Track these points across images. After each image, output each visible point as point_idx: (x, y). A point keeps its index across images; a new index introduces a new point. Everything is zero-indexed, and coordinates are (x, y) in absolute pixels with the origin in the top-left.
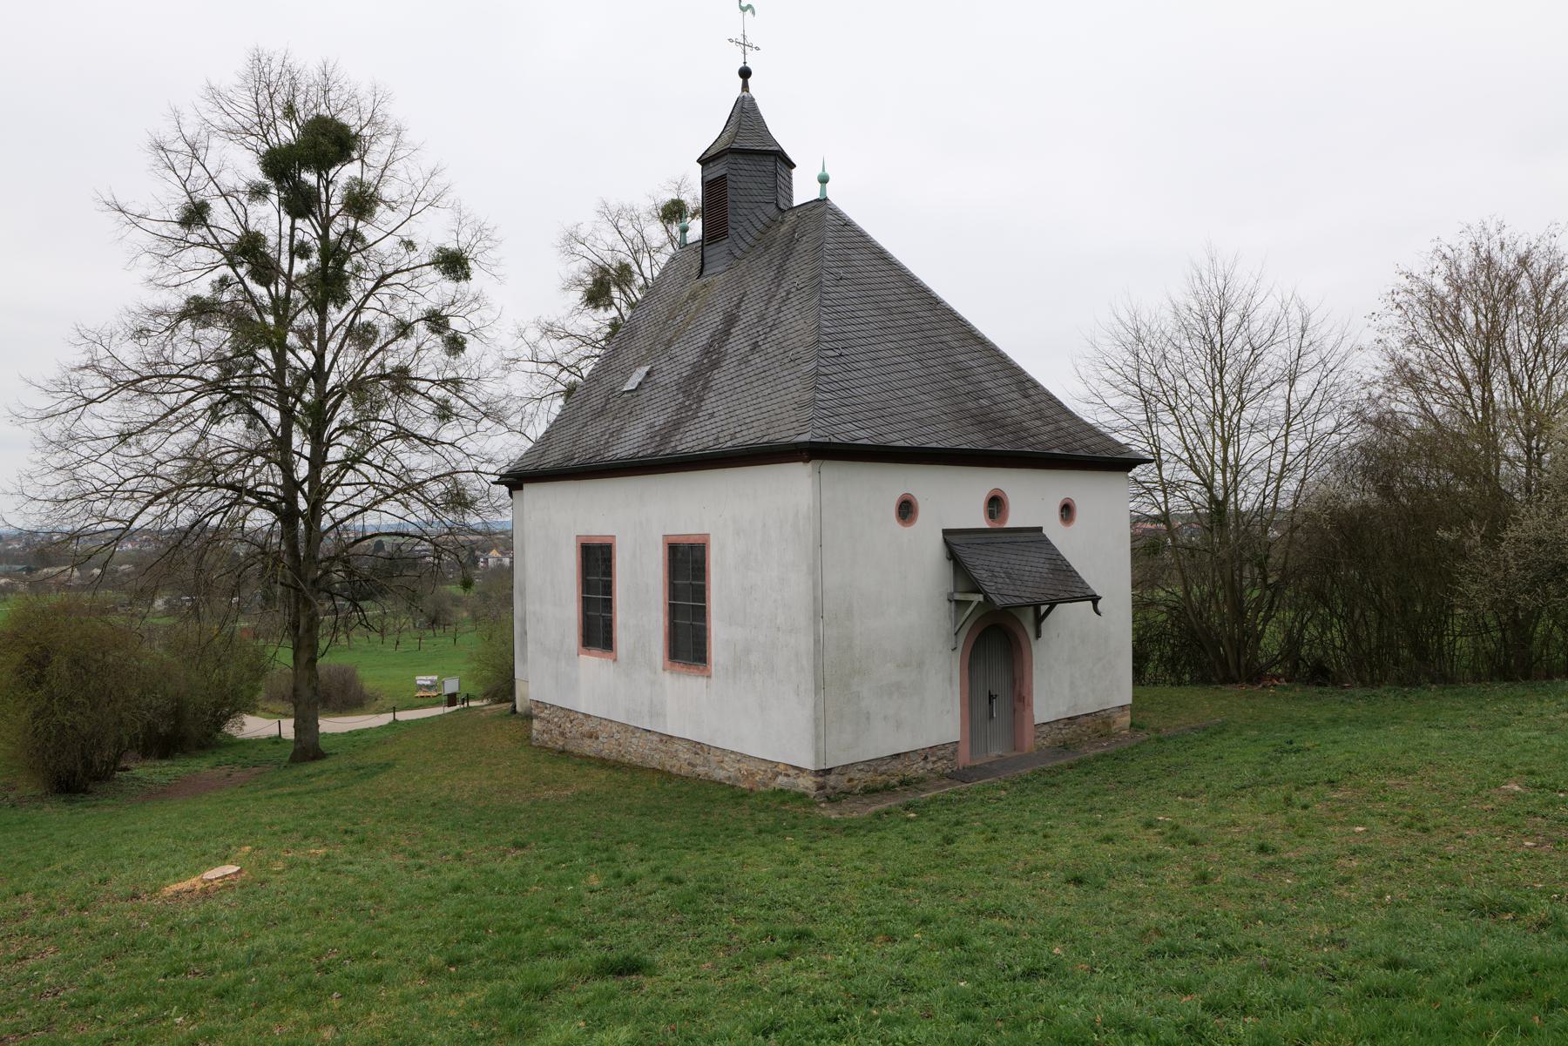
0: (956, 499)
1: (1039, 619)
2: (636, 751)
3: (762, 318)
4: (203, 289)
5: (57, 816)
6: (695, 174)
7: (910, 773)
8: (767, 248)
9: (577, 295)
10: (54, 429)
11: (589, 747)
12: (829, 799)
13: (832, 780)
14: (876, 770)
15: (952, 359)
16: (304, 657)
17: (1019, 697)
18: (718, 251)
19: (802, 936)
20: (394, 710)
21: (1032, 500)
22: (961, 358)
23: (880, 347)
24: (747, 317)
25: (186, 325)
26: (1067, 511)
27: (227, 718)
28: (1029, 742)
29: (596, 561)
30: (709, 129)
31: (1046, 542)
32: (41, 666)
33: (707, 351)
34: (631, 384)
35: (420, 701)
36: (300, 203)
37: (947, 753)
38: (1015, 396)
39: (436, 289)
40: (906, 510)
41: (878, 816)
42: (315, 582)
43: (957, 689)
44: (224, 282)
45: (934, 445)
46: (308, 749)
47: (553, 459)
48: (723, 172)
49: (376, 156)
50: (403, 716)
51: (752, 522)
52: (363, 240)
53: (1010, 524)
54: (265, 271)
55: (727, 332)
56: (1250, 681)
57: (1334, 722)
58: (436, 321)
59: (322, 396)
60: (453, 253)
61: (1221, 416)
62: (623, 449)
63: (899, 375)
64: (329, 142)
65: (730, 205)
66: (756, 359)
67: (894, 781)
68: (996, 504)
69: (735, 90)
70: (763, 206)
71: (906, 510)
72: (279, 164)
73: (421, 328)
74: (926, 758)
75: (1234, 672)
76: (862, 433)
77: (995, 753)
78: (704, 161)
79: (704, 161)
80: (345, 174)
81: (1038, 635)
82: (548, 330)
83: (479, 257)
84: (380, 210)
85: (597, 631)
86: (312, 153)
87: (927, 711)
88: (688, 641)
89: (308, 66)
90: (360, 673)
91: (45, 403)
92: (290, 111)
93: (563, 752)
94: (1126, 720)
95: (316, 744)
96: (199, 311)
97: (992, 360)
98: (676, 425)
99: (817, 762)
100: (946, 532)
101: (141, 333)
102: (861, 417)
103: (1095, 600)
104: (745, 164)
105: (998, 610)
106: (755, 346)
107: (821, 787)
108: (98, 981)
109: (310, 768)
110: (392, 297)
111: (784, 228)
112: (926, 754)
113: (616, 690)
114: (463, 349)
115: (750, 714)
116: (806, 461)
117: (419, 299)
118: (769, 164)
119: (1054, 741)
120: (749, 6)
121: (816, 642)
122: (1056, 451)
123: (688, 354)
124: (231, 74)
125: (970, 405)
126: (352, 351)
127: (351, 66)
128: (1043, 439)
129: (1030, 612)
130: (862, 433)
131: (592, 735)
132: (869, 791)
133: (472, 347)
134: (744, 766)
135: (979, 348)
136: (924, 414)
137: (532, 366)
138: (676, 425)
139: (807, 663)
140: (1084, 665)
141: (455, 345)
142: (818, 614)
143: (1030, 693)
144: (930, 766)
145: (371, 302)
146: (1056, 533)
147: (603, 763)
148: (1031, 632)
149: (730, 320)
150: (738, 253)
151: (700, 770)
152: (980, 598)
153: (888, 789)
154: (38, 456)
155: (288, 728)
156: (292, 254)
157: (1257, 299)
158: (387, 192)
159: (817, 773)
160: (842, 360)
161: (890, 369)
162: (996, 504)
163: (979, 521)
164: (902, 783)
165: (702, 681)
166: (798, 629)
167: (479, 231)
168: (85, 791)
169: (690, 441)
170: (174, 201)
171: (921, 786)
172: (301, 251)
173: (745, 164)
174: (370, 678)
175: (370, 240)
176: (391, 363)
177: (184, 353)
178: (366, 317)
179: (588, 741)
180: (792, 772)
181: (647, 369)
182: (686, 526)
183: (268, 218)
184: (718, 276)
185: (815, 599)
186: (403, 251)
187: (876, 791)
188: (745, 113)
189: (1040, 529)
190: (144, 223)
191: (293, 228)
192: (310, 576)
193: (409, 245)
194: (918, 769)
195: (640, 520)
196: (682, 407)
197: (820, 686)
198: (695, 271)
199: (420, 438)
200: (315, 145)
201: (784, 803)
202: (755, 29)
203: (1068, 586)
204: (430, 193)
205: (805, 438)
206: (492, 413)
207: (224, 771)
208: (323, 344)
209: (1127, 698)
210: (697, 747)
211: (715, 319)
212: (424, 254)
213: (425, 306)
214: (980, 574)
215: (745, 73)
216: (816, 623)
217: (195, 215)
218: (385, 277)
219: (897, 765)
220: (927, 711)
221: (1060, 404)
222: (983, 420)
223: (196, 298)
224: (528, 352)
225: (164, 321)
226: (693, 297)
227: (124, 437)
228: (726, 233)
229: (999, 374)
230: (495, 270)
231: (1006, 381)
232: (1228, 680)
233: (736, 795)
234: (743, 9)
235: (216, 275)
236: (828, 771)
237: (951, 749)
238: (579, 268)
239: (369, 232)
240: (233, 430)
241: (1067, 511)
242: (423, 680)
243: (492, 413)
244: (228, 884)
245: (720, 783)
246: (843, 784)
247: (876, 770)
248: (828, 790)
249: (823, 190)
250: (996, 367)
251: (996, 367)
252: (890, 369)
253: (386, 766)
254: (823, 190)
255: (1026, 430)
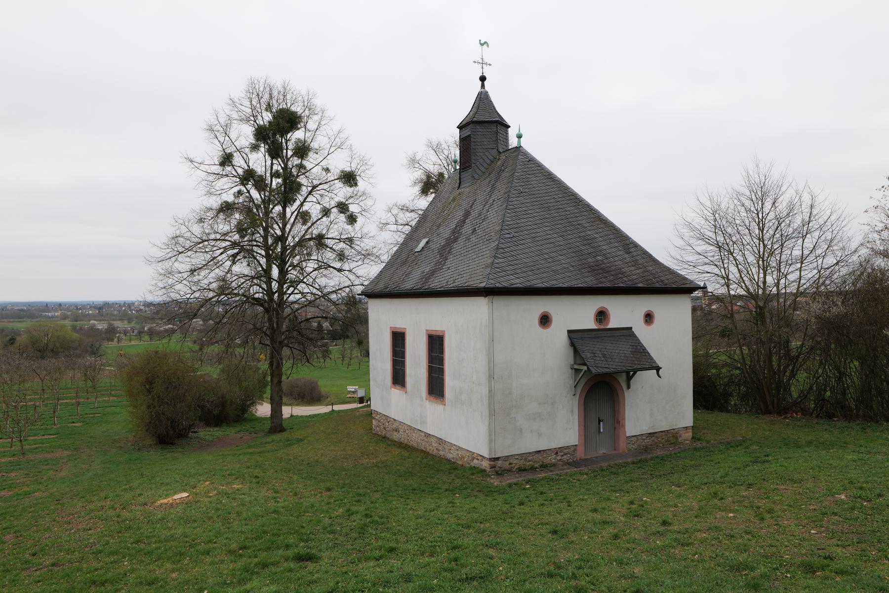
0: (579, 314)
1: (629, 378)
2: (415, 440)
3: (480, 215)
4: (230, 198)
5: (154, 455)
6: (455, 134)
7: (547, 461)
8: (490, 174)
9: (417, 189)
10: (160, 267)
11: (395, 436)
12: (497, 474)
13: (499, 463)
14: (526, 459)
15: (583, 234)
16: (276, 380)
17: (617, 421)
18: (466, 175)
19: (391, 550)
20: (332, 405)
21: (624, 313)
22: (589, 233)
23: (539, 230)
24: (474, 214)
25: (221, 216)
26: (649, 318)
27: (249, 406)
28: (623, 446)
29: (398, 338)
30: (463, 109)
31: (633, 335)
32: (151, 383)
33: (454, 232)
34: (419, 248)
35: (349, 400)
36: (275, 152)
37: (570, 451)
38: (621, 253)
39: (341, 192)
40: (545, 320)
41: (510, 486)
42: (281, 343)
43: (577, 417)
44: (240, 193)
45: (561, 285)
46: (276, 425)
47: (380, 287)
48: (469, 133)
49: (311, 125)
50: (337, 408)
51: (464, 324)
52: (305, 168)
53: (610, 326)
54: (260, 184)
55: (464, 221)
56: (779, 414)
57: (810, 443)
58: (342, 207)
59: (284, 249)
60: (349, 173)
61: (763, 258)
62: (408, 285)
63: (548, 246)
64: (288, 120)
65: (472, 151)
66: (473, 238)
67: (537, 465)
68: (602, 315)
69: (478, 89)
70: (490, 151)
71: (545, 320)
72: (262, 134)
73: (335, 210)
74: (556, 453)
75: (770, 407)
76: (517, 281)
77: (602, 451)
78: (460, 127)
79: (460, 127)
80: (298, 135)
81: (629, 387)
82: (404, 209)
83: (362, 174)
84: (311, 154)
85: (399, 378)
86: (279, 128)
87: (560, 428)
88: (436, 387)
89: (277, 82)
90: (321, 383)
91: (159, 254)
92: (269, 107)
93: (384, 437)
94: (689, 434)
95: (281, 425)
96: (226, 208)
97: (610, 232)
98: (433, 272)
99: (490, 454)
100: (569, 332)
101: (201, 220)
102: (518, 271)
103: (658, 369)
104: (483, 129)
105: (603, 374)
106: (474, 230)
107: (492, 467)
108: (107, 543)
109: (278, 437)
110: (322, 196)
111: (499, 163)
112: (556, 451)
113: (402, 407)
114: (356, 221)
115: (460, 426)
116: (486, 296)
117: (333, 196)
118: (493, 128)
119: (639, 446)
120: (486, 43)
121: (490, 391)
122: (640, 285)
123: (446, 232)
124: (239, 92)
125: (590, 260)
126: (299, 225)
127: (300, 80)
128: (635, 277)
129: (624, 375)
130: (517, 281)
131: (397, 430)
132: (521, 470)
133: (360, 220)
134: (460, 453)
135: (602, 226)
136: (558, 267)
137: (394, 228)
138: (433, 272)
139: (485, 401)
140: (661, 402)
141: (352, 219)
142: (491, 376)
143: (624, 419)
144: (559, 458)
145: (310, 198)
146: (641, 331)
147: (401, 445)
148: (624, 386)
149: (467, 214)
150: (476, 176)
151: (441, 453)
152: (585, 368)
153: (533, 469)
154: (154, 282)
155: (287, 411)
156: (272, 176)
157: (783, 189)
158: (314, 145)
159: (490, 459)
160: (514, 239)
161: (542, 242)
162: (602, 315)
163: (591, 325)
164: (541, 466)
165: (442, 407)
166: (484, 382)
167: (364, 162)
168: (172, 444)
169: (436, 283)
170: (216, 156)
171: (552, 469)
172: (276, 175)
173: (483, 129)
174: (325, 386)
175: (308, 169)
176: (316, 232)
177: (223, 227)
178: (305, 208)
179: (395, 433)
180: (480, 458)
181: (426, 240)
182: (436, 327)
183: (260, 161)
184: (466, 190)
185: (489, 369)
186: (324, 173)
187: (525, 470)
188: (483, 101)
189: (631, 328)
190: (203, 167)
191: (272, 164)
192: (278, 340)
193: (327, 170)
194: (552, 459)
195: (418, 319)
196: (438, 263)
197: (492, 414)
198: (457, 185)
199: (335, 268)
200: (278, 124)
201: (473, 474)
202: (488, 54)
203: (642, 360)
204: (338, 142)
205: (483, 285)
206: (366, 255)
207: (239, 435)
208: (285, 225)
209: (689, 422)
210: (440, 441)
211: (460, 213)
212: (335, 172)
213: (337, 199)
214: (586, 355)
215: (483, 79)
216: (490, 381)
217: (227, 160)
218: (314, 187)
219: (539, 457)
220: (560, 428)
221: (650, 256)
222: (595, 269)
223: (226, 202)
224: (394, 220)
225: (211, 214)
226: (454, 200)
227: (192, 271)
228: (470, 166)
229: (612, 241)
230: (371, 180)
231: (616, 244)
232: (767, 412)
233: (452, 467)
234: (482, 45)
235: (236, 189)
236: (498, 459)
237: (572, 449)
238: (419, 174)
239: (308, 164)
240: (242, 268)
241: (649, 318)
242: (351, 388)
243: (366, 255)
244: (182, 501)
245: (449, 461)
246: (506, 465)
247: (526, 459)
248: (497, 469)
249: (519, 142)
250: (611, 237)
251: (611, 237)
252: (542, 242)
253: (300, 440)
254: (519, 142)
255: (623, 273)
